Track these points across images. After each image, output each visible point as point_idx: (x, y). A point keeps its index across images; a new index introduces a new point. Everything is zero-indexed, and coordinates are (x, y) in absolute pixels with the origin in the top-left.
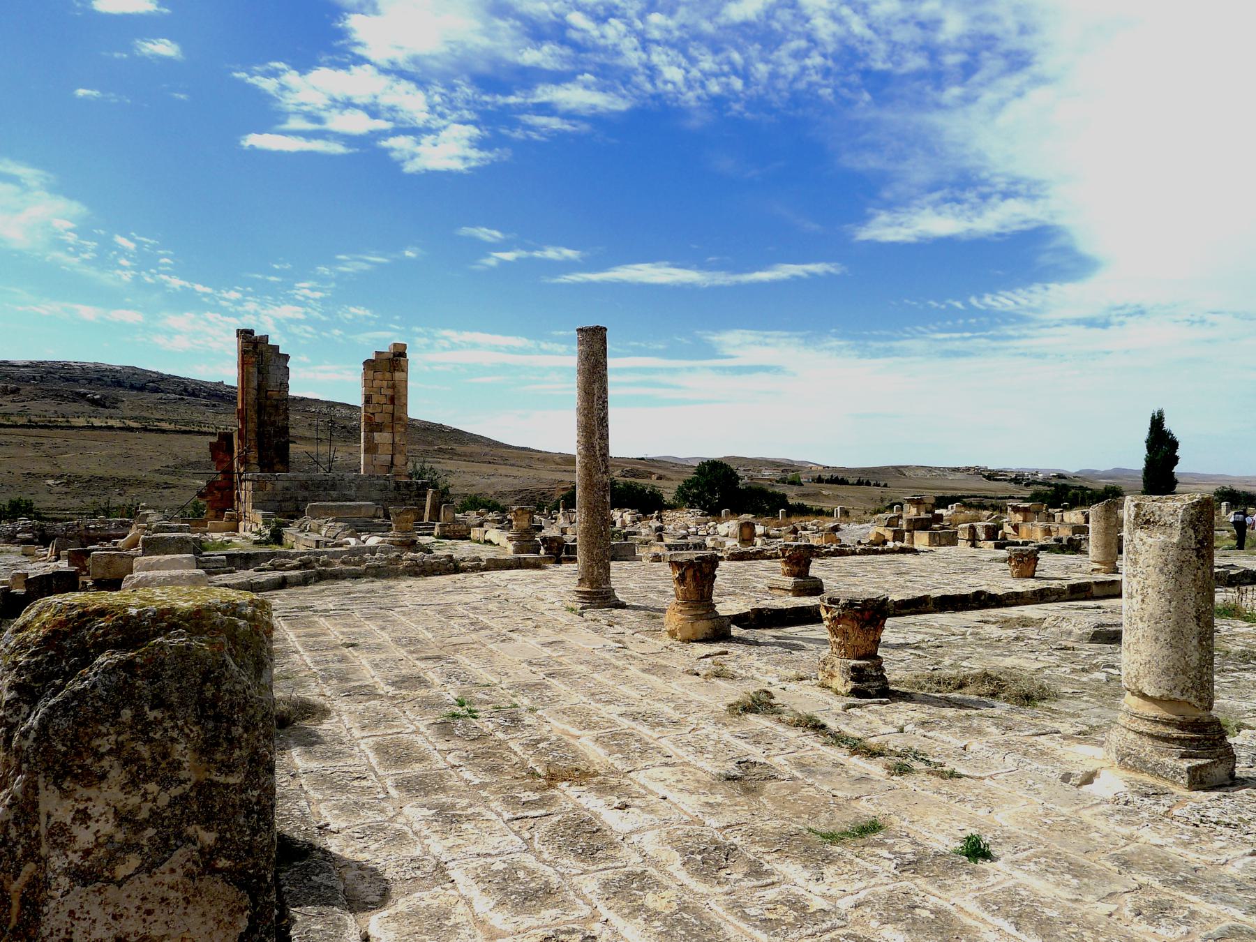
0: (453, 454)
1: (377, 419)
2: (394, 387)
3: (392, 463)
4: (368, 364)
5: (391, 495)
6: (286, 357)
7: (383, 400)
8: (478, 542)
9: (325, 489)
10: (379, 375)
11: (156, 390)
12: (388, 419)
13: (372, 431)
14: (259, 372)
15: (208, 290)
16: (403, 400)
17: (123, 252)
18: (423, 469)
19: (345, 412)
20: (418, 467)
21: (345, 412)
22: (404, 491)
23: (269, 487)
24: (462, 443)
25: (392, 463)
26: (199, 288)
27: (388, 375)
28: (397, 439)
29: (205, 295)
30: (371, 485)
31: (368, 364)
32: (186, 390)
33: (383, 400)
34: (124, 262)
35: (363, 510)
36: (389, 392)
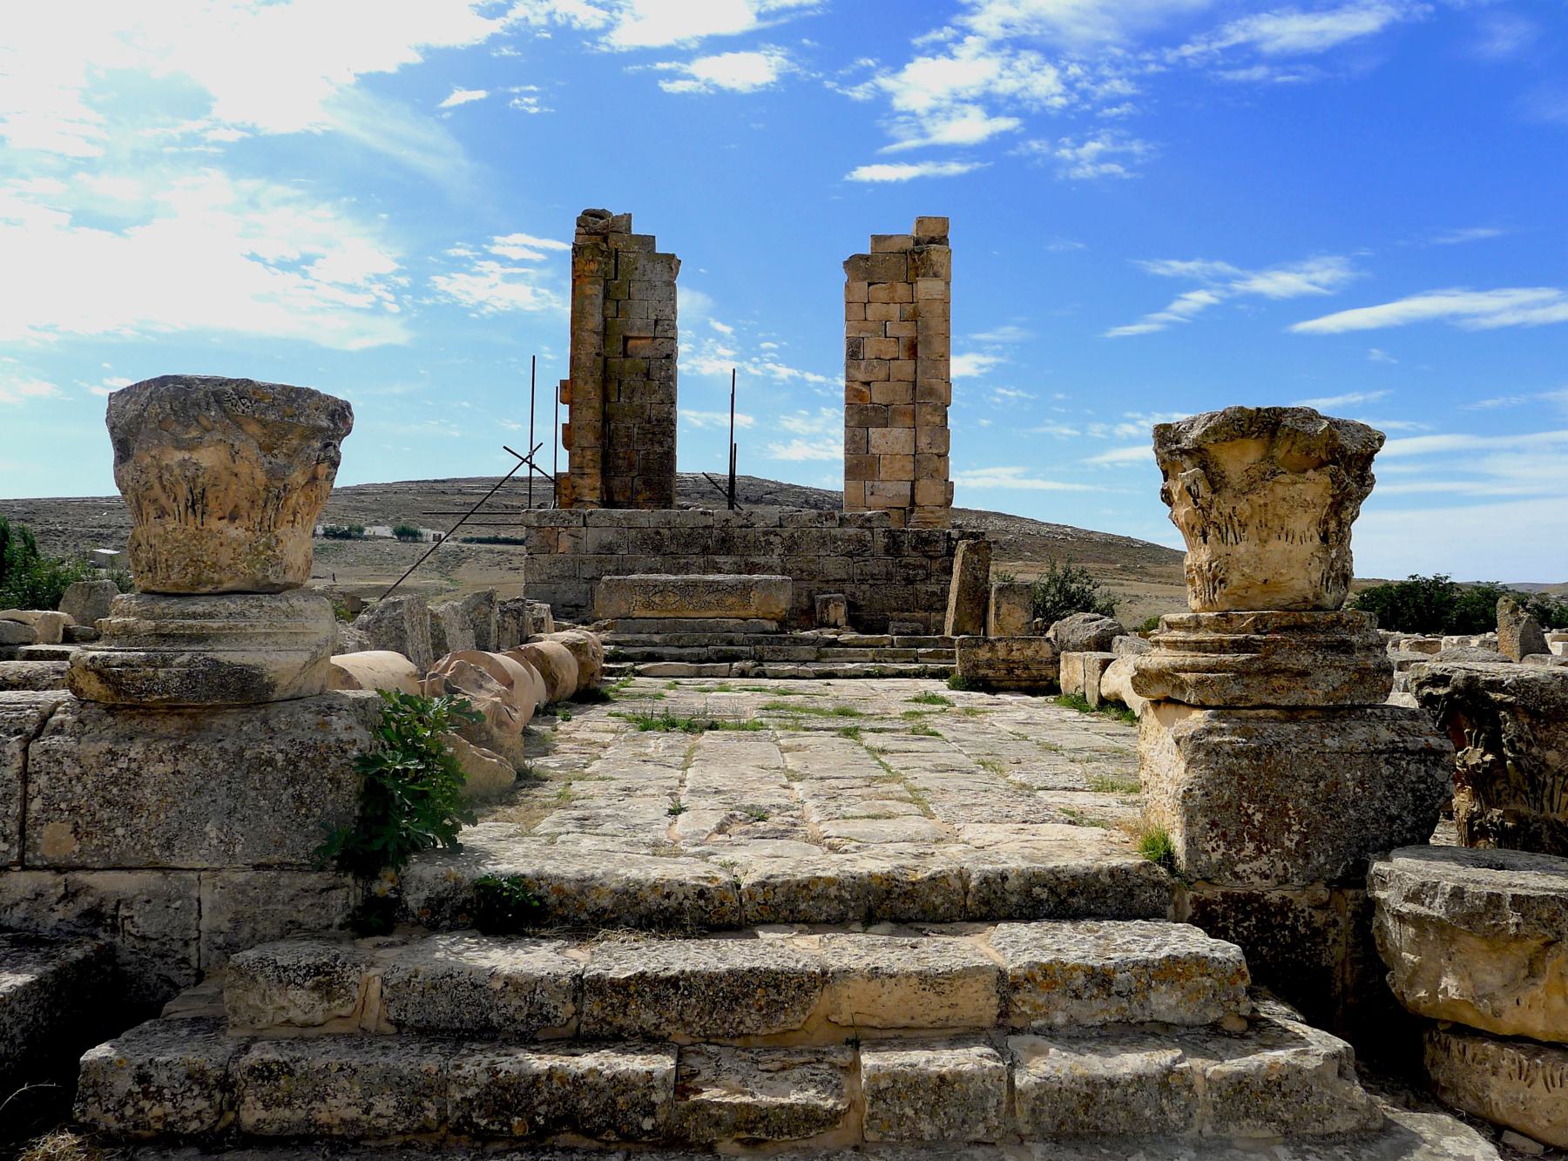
0: (1143, 574)
1: (878, 396)
2: (915, 317)
3: (913, 503)
4: (856, 265)
5: (877, 566)
6: (671, 262)
7: (891, 350)
8: (1079, 703)
9: (705, 550)
10: (880, 292)
11: (774, 502)
12: (901, 396)
13: (865, 425)
14: (606, 297)
15: (820, 378)
16: (937, 346)
17: (719, 337)
18: (1067, 572)
19: (1000, 524)
20: (1059, 572)
21: (1000, 524)
22: (913, 558)
23: (565, 543)
24: (1158, 562)
25: (913, 503)
26: (810, 377)
27: (902, 290)
28: (923, 441)
29: (818, 385)
30: (823, 541)
31: (856, 265)
32: (807, 502)
33: (891, 350)
34: (721, 351)
35: (755, 597)
36: (906, 331)
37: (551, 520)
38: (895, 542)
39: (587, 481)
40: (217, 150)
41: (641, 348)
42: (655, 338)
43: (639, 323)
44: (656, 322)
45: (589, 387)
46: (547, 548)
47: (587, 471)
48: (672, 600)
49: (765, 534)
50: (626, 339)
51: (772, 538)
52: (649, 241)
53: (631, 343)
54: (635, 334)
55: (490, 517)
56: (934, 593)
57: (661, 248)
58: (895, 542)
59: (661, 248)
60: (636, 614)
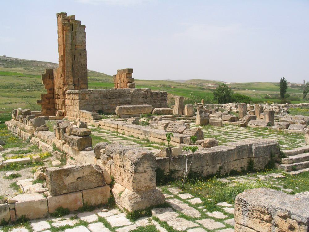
9: (116, 98)
35: (146, 109)
37: (84, 92)
38: (152, 94)
39: (70, 79)
40: (210, 92)
41: (79, 48)
42: (82, 45)
43: (78, 42)
44: (82, 41)
45: (69, 57)
46: (83, 99)
47: (70, 77)
48: (132, 111)
49: (128, 94)
50: (75, 45)
51: (129, 94)
52: (79, 22)
53: (76, 46)
54: (78, 44)
55: (233, 131)
56: (159, 104)
57: (82, 24)
58: (152, 94)
59: (82, 24)
60: (125, 114)
